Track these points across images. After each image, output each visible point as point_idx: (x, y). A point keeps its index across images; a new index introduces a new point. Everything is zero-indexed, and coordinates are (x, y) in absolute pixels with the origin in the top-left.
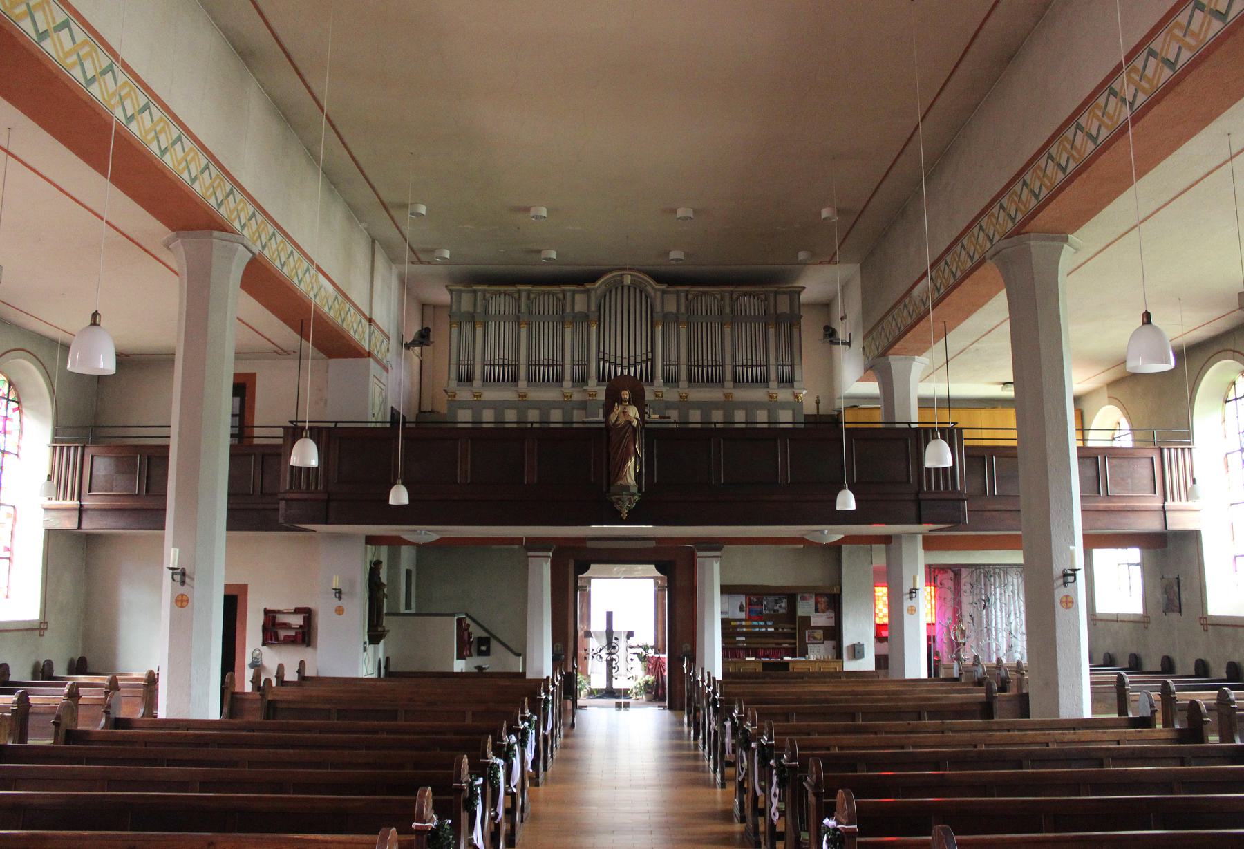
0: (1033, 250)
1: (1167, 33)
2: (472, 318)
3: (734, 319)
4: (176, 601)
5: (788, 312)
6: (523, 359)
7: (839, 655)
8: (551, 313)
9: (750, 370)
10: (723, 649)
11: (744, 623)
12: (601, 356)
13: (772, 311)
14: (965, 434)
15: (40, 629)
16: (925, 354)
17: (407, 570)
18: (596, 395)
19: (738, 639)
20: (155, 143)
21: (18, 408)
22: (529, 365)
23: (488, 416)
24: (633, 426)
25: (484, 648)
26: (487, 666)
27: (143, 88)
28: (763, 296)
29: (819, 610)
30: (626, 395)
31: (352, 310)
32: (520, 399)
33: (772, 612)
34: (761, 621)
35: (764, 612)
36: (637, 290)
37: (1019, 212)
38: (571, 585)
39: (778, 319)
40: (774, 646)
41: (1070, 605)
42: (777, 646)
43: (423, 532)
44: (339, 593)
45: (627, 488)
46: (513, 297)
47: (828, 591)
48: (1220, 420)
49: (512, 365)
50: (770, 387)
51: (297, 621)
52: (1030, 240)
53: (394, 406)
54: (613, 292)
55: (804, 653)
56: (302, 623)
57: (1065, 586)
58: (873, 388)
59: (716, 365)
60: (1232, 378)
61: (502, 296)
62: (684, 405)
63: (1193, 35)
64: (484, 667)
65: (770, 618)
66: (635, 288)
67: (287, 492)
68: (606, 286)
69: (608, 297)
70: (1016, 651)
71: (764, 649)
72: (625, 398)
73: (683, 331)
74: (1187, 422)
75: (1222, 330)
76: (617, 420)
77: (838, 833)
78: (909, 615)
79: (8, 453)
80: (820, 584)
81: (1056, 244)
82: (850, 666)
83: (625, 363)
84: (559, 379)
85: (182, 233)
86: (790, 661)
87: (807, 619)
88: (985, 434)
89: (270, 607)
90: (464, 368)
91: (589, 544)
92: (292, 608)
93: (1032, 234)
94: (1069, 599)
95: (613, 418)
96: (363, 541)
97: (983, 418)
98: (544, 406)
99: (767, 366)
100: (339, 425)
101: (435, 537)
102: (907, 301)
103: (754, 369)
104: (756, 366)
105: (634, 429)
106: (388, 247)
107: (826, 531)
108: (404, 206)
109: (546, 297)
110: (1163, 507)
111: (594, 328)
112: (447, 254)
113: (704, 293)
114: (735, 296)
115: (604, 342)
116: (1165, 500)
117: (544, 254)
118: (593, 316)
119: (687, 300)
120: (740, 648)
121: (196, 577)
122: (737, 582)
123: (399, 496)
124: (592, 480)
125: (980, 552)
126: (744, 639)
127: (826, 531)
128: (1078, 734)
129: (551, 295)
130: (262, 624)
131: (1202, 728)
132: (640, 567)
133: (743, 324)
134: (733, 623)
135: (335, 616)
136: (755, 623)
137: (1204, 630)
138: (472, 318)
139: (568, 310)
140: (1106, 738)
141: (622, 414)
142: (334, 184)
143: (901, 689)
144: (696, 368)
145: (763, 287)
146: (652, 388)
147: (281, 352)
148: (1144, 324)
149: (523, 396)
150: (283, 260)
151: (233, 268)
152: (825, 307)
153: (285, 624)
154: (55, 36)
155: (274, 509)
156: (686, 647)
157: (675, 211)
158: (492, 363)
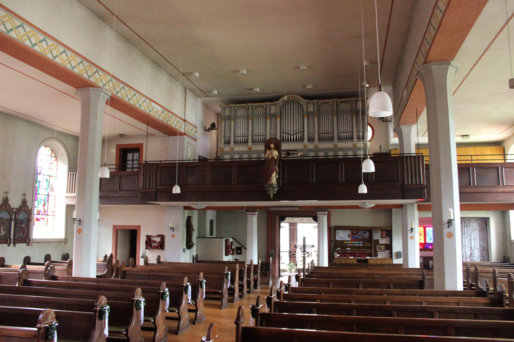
0: (433, 70)
2: (229, 118)
3: (338, 113)
7: (391, 257)
8: (261, 114)
11: (350, 242)
12: (282, 131)
13: (354, 109)
15: (65, 242)
19: (347, 249)
20: (127, 97)
21: (56, 160)
25: (239, 251)
27: (42, 33)
28: (350, 103)
30: (272, 146)
31: (173, 116)
33: (362, 238)
35: (359, 238)
38: (277, 226)
40: (362, 252)
41: (451, 236)
42: (364, 252)
43: (199, 204)
44: (173, 229)
45: (272, 185)
47: (386, 229)
51: (158, 240)
53: (200, 155)
55: (376, 255)
62: (317, 149)
65: (361, 240)
67: (141, 189)
70: (474, 256)
71: (358, 253)
76: (268, 156)
78: (411, 240)
79: (51, 176)
81: (445, 66)
82: (396, 261)
86: (369, 259)
87: (378, 241)
89: (148, 234)
90: (227, 138)
91: (271, 209)
92: (156, 235)
94: (451, 234)
96: (183, 209)
99: (352, 132)
100: (162, 162)
101: (374, 205)
103: (347, 134)
105: (275, 160)
106: (192, 91)
107: (367, 203)
108: (191, 74)
109: (260, 107)
114: (338, 103)
118: (279, 115)
119: (318, 105)
120: (348, 253)
121: (84, 222)
122: (347, 225)
123: (177, 190)
126: (350, 249)
128: (438, 298)
130: (145, 240)
131: (503, 299)
132: (306, 219)
133: (342, 115)
134: (345, 242)
135: (171, 238)
136: (355, 242)
138: (229, 118)
139: (268, 112)
142: (160, 67)
144: (322, 134)
146: (302, 143)
149: (250, 149)
151: (100, 101)
153: (154, 241)
154: (121, 92)
155: (136, 196)
157: (299, 68)
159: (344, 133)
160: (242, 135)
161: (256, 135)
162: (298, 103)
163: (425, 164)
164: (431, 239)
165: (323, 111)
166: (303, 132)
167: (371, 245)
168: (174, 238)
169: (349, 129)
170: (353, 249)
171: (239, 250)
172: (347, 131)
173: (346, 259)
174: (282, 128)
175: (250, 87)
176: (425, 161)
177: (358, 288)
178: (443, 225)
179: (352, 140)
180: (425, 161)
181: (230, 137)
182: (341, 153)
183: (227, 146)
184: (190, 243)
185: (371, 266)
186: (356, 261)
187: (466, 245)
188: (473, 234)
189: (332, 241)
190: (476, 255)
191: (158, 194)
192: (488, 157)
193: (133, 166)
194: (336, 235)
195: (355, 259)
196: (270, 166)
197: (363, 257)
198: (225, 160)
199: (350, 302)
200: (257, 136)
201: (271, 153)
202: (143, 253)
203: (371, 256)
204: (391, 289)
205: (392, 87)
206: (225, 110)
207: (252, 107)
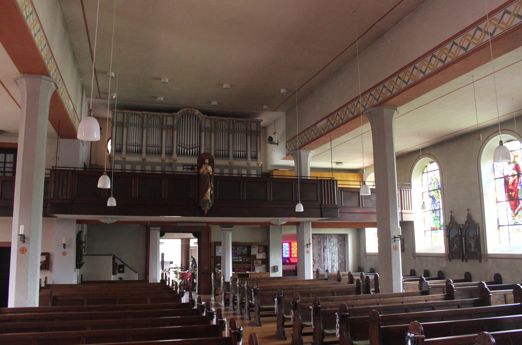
1: (463, 37)
4: (20, 250)
5: (256, 130)
9: (239, 153)
10: (233, 268)
12: (178, 144)
13: (249, 129)
14: (339, 182)
16: (314, 150)
18: (176, 161)
22: (147, 147)
23: (128, 167)
24: (210, 175)
25: (121, 270)
26: (124, 278)
28: (245, 123)
29: (260, 252)
30: (207, 161)
32: (143, 161)
34: (237, 257)
36: (194, 117)
39: (252, 132)
40: (242, 267)
42: (243, 267)
43: (110, 218)
45: (208, 201)
46: (140, 116)
48: (421, 180)
49: (139, 146)
50: (248, 160)
52: (384, 108)
53: (85, 162)
54: (184, 117)
55: (254, 270)
56: (45, 260)
57: (395, 242)
58: (291, 163)
59: (226, 150)
60: (426, 164)
61: (136, 116)
63: (476, 39)
64: (122, 278)
66: (193, 116)
68: (181, 114)
69: (181, 119)
71: (238, 268)
72: (207, 163)
73: (213, 135)
74: (410, 181)
75: (426, 146)
76: (203, 172)
77: (416, 339)
78: (307, 254)
80: (260, 241)
81: (393, 110)
82: (272, 275)
84: (160, 153)
85: (26, 75)
87: (255, 256)
90: (118, 146)
91: (179, 225)
93: (385, 106)
95: (202, 171)
96: (75, 222)
98: (153, 164)
99: (247, 151)
100: (76, 169)
101: (115, 221)
102: (313, 128)
104: (242, 151)
105: (211, 176)
107: (280, 220)
108: (105, 73)
109: (155, 117)
110: (401, 212)
111: (176, 132)
113: (222, 120)
114: (234, 122)
115: (180, 136)
116: (402, 209)
117: (158, 99)
119: (215, 122)
123: (300, 208)
124: (191, 197)
125: (323, 229)
127: (280, 220)
129: (157, 117)
133: (237, 134)
137: (414, 258)
139: (165, 123)
140: (422, 299)
141: (205, 169)
143: (309, 284)
145: (246, 119)
146: (247, 161)
148: (500, 145)
156: (206, 268)
157: (222, 85)
158: (150, 145)
159: (238, 151)
164: (287, 254)
167: (249, 260)
168: (65, 256)
171: (121, 268)
174: (178, 141)
177: (309, 297)
178: (391, 240)
179: (228, 158)
181: (122, 145)
184: (81, 262)
189: (212, 257)
192: (351, 183)
193: (4, 169)
194: (217, 250)
195: (237, 274)
197: (243, 272)
199: (378, 305)
201: (206, 169)
203: (250, 271)
204: (335, 296)
205: (285, 112)
207: (147, 116)
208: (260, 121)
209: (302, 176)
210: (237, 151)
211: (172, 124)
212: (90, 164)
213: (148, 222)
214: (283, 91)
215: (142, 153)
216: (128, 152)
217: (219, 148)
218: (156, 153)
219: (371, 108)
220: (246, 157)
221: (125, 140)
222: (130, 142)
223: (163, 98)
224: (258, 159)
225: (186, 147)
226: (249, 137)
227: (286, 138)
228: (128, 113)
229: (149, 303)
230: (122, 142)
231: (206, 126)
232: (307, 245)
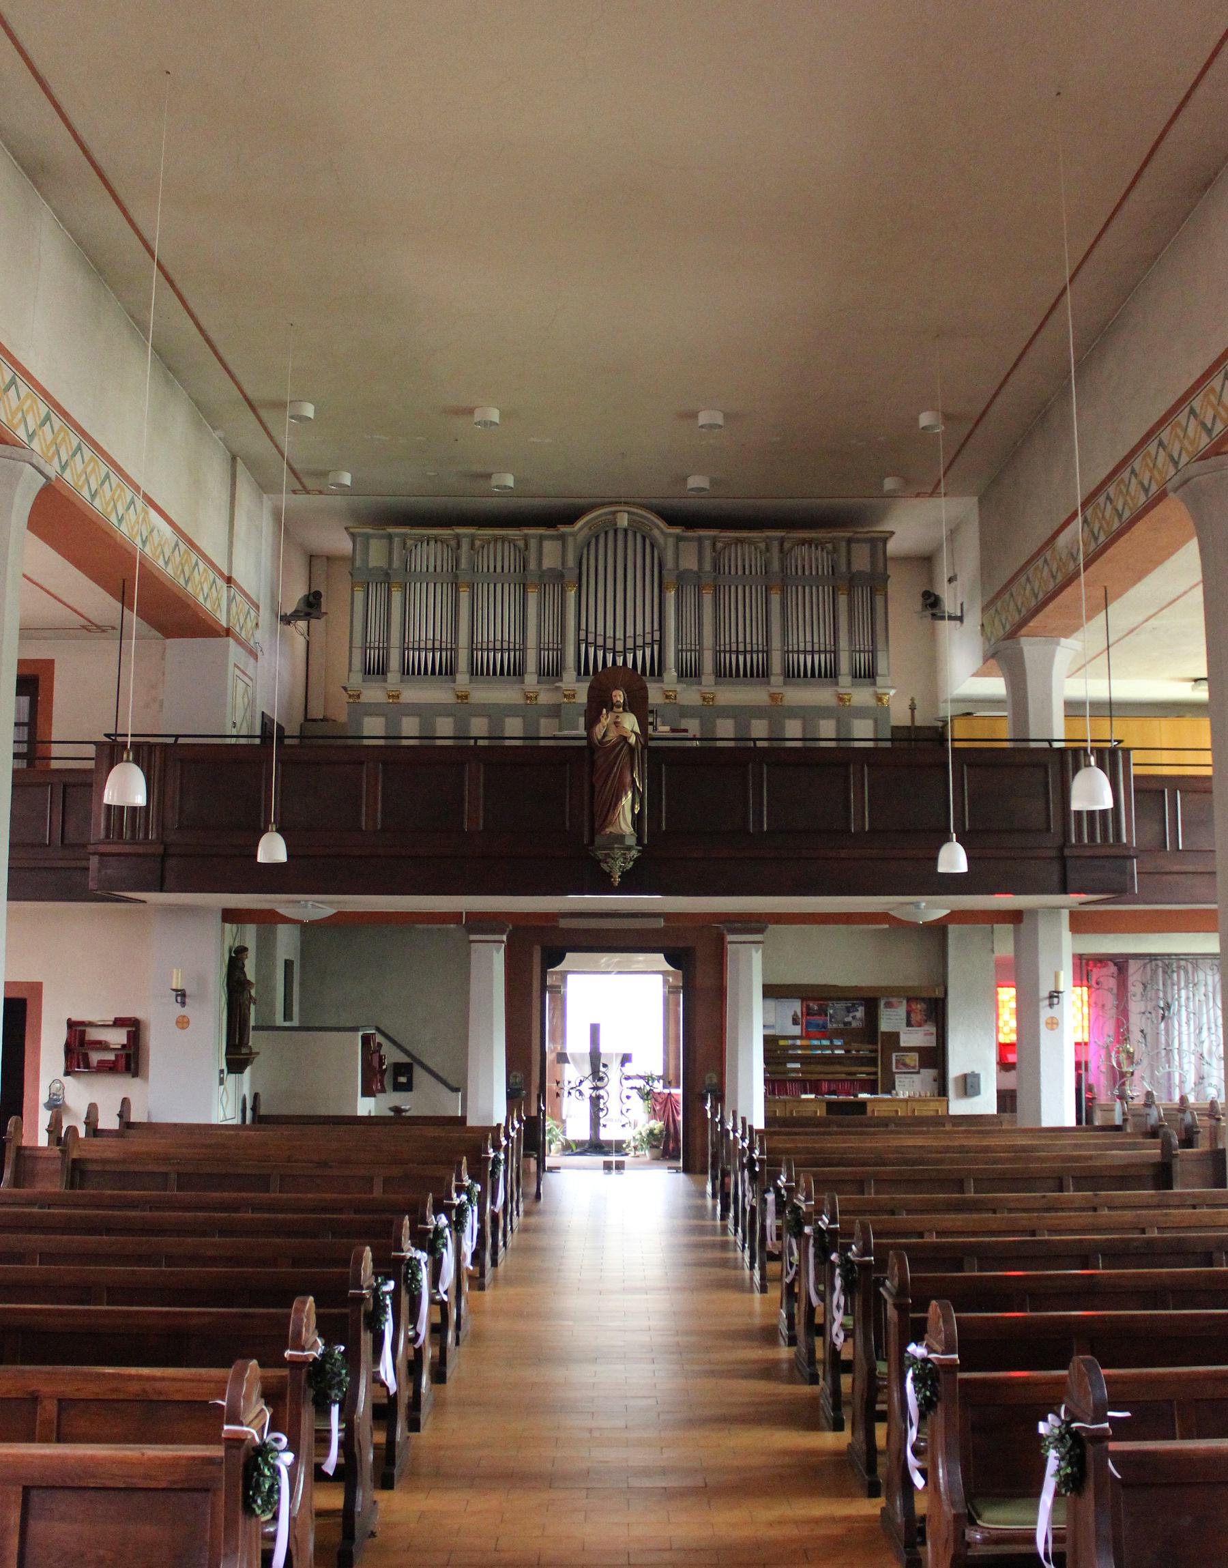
2: (386, 578)
6: (463, 640)
7: (943, 1091)
11: (798, 1042)
12: (583, 636)
13: (843, 568)
14: (1135, 757)
17: (286, 961)
18: (574, 696)
19: (790, 1066)
24: (630, 745)
25: (403, 1079)
26: (407, 1107)
28: (830, 546)
30: (619, 696)
35: (829, 1026)
37: (1126, 508)
40: (843, 1076)
44: (181, 995)
45: (620, 838)
47: (924, 995)
51: (118, 1038)
55: (890, 1087)
56: (125, 1041)
58: (996, 686)
61: (432, 543)
62: (709, 711)
65: (838, 1033)
67: (101, 842)
70: (1210, 1085)
71: (829, 1081)
73: (708, 598)
76: (605, 735)
82: (958, 1107)
83: (619, 647)
84: (518, 671)
87: (895, 1036)
88: (1165, 757)
90: (373, 654)
91: (564, 923)
92: (110, 1018)
95: (599, 731)
96: (219, 915)
97: (1163, 732)
98: (496, 713)
99: (835, 652)
100: (181, 741)
101: (329, 911)
102: (1048, 555)
104: (864, 652)
105: (632, 749)
106: (254, 466)
107: (923, 904)
108: (280, 405)
111: (571, 594)
112: (347, 479)
113: (739, 541)
114: (787, 545)
118: (571, 576)
126: (798, 1066)
132: (641, 957)
134: (782, 1043)
136: (816, 1042)
138: (386, 578)
139: (532, 565)
147: (92, 628)
149: (463, 697)
150: (94, 487)
152: (925, 561)
153: (100, 1042)
157: (693, 415)
158: (728, 648)
160: (430, 645)
161: (485, 646)
162: (644, 538)
163: (1135, 777)
165: (733, 572)
166: (661, 643)
167: (871, 1051)
169: (822, 641)
170: (812, 1068)
172: (816, 648)
173: (789, 1101)
174: (583, 626)
175: (477, 468)
176: (1134, 765)
180: (1134, 765)
182: (793, 729)
183: (374, 684)
184: (244, 1051)
185: (897, 1125)
186: (824, 1108)
187: (1185, 1046)
188: (1205, 1011)
190: (1214, 1081)
191: (171, 863)
195: (822, 1101)
196: (610, 773)
198: (366, 742)
199: (1034, 1235)
200: (488, 649)
201: (616, 724)
202: (53, 1091)
203: (874, 1092)
205: (975, 499)
206: (368, 543)
208: (883, 535)
209: (1032, 737)
210: (798, 652)
211: (385, 566)
212: (306, 720)
213: (462, 913)
214: (925, 419)
215: (873, 677)
216: (407, 671)
217: (802, 645)
218: (802, 674)
219: (1197, 460)
220: (832, 674)
221: (398, 636)
222: (414, 635)
223: (512, 477)
224: (878, 678)
225: (610, 644)
226: (843, 600)
227: (983, 596)
228: (405, 535)
229: (378, 1192)
230: (456, 638)
231: (681, 568)
232: (1051, 997)
